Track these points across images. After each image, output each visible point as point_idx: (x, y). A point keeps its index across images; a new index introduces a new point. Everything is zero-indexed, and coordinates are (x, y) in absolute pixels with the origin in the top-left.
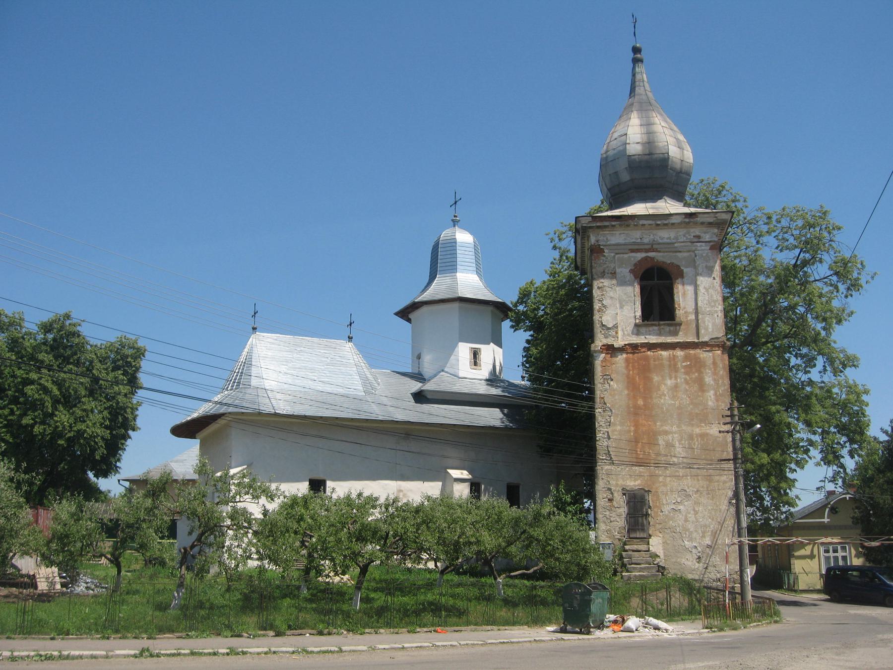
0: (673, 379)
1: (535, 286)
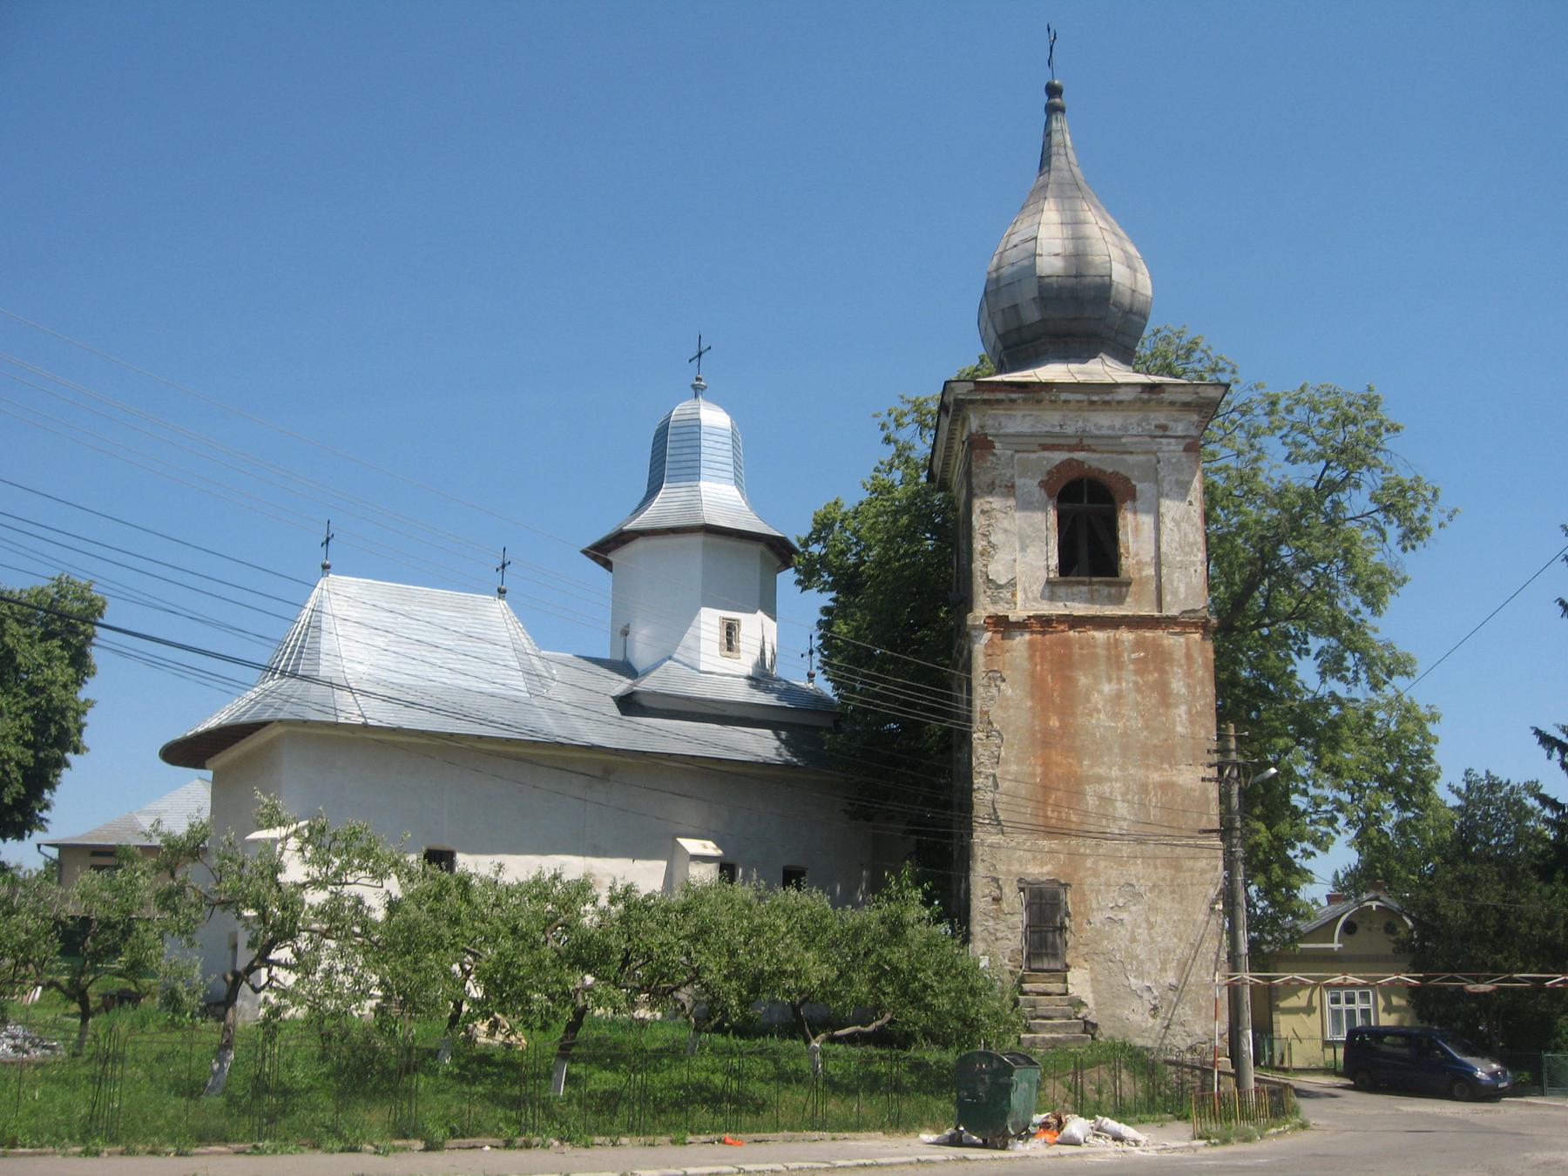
0: (1115, 681)
1: (843, 510)
